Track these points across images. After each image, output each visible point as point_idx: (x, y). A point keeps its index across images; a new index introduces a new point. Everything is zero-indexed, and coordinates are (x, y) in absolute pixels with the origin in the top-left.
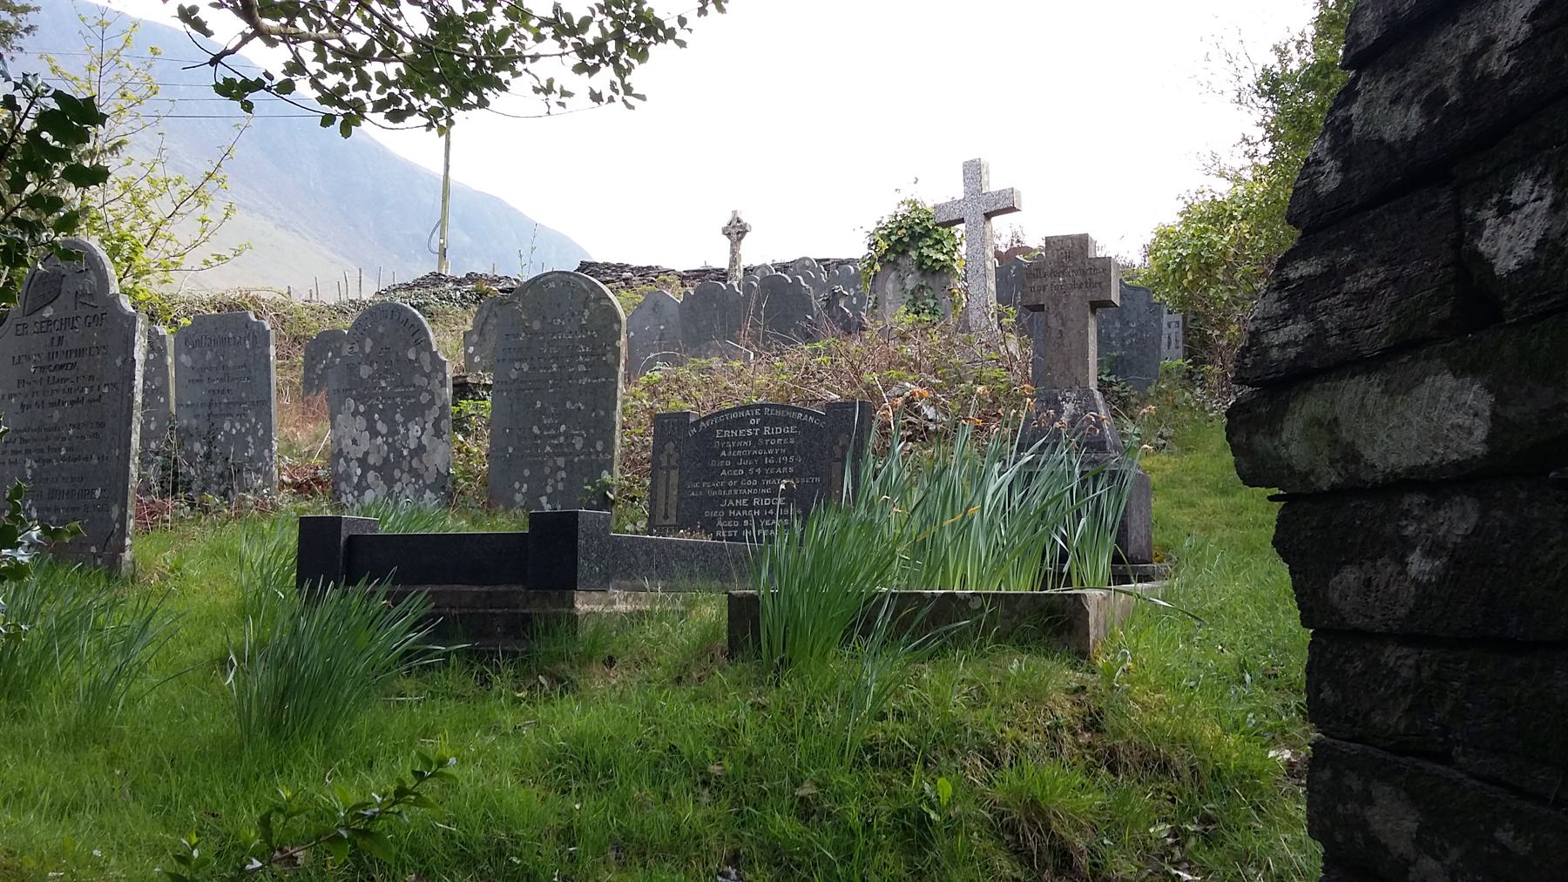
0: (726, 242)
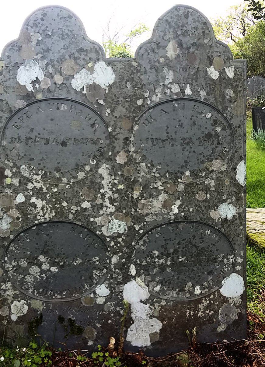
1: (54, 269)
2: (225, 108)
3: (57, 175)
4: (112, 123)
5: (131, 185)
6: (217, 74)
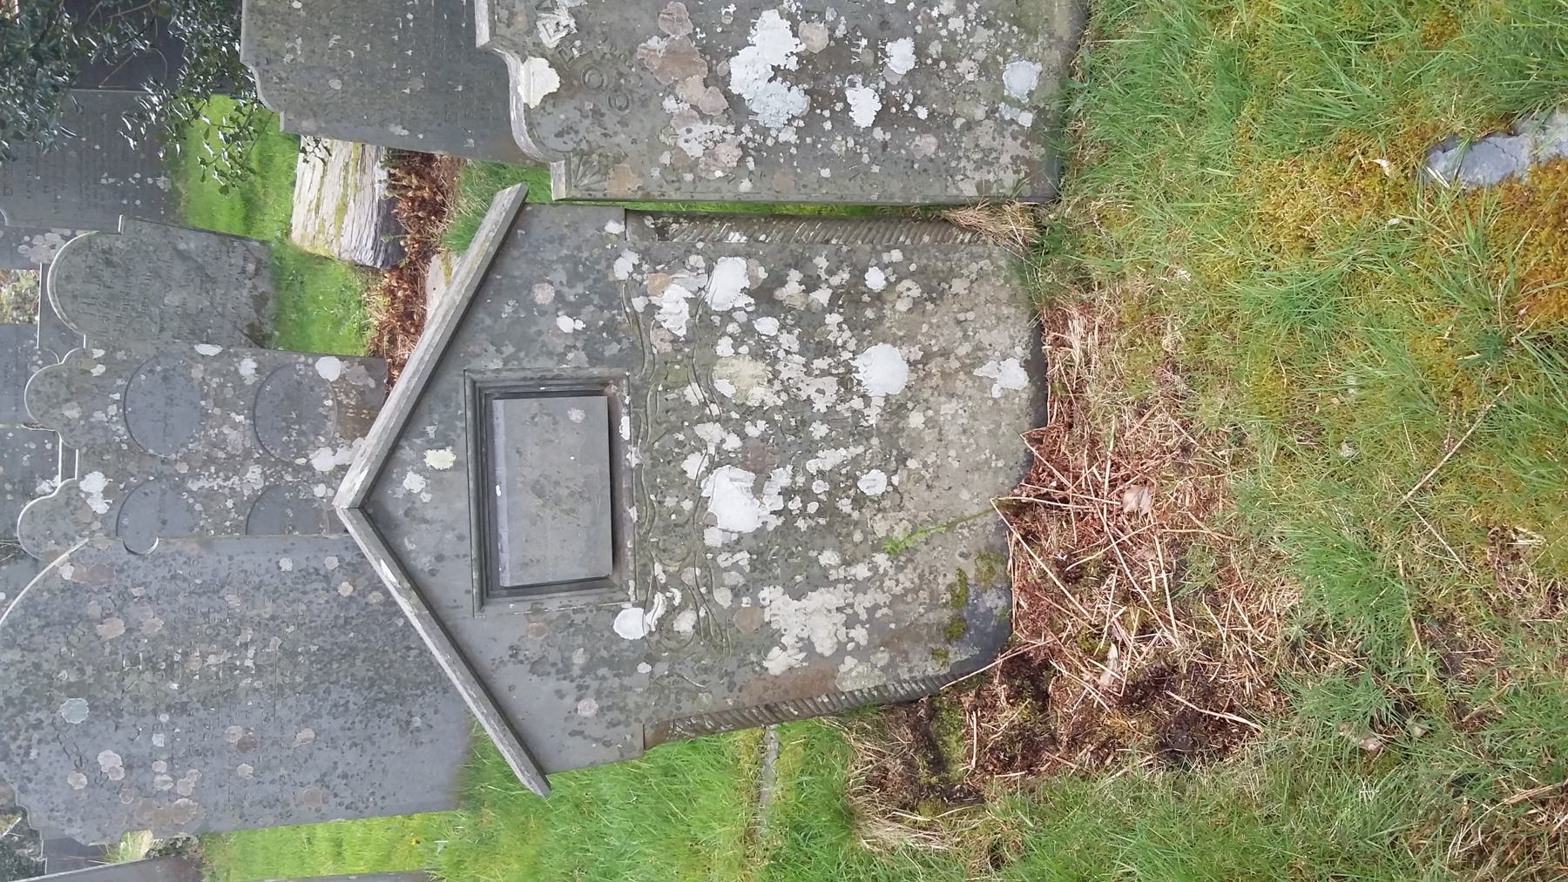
2: (137, 361)
5: (211, 460)
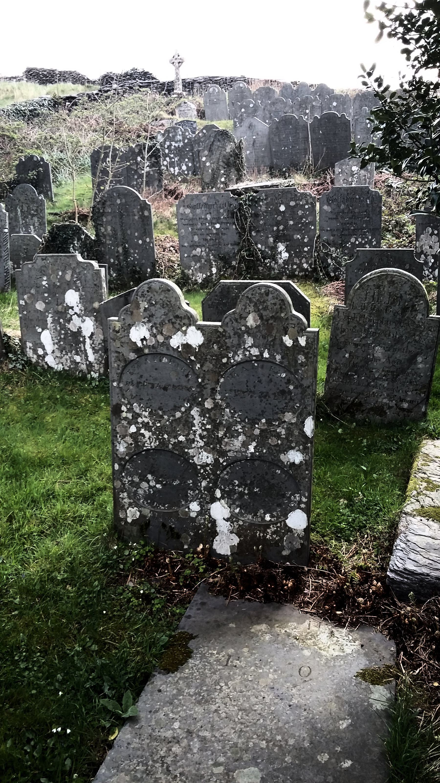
0: (173, 68)
1: (158, 486)
2: (297, 371)
3: (160, 413)
4: (201, 375)
5: (216, 426)
6: (291, 342)
